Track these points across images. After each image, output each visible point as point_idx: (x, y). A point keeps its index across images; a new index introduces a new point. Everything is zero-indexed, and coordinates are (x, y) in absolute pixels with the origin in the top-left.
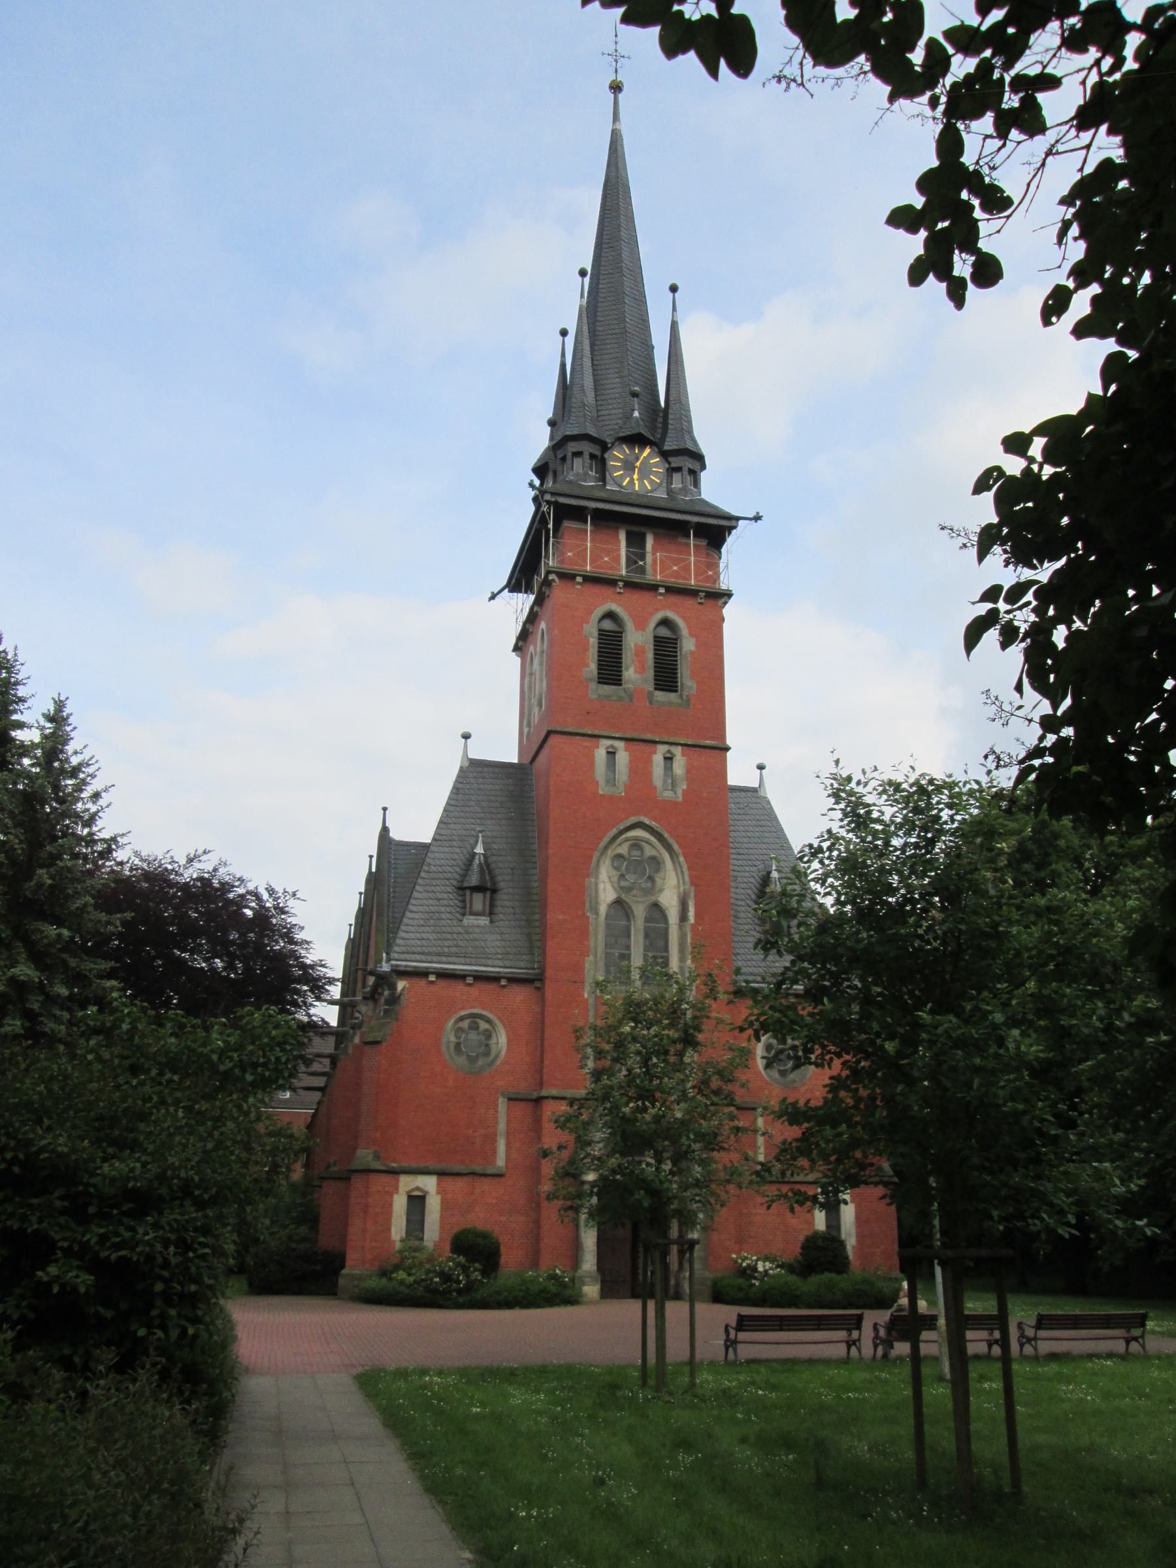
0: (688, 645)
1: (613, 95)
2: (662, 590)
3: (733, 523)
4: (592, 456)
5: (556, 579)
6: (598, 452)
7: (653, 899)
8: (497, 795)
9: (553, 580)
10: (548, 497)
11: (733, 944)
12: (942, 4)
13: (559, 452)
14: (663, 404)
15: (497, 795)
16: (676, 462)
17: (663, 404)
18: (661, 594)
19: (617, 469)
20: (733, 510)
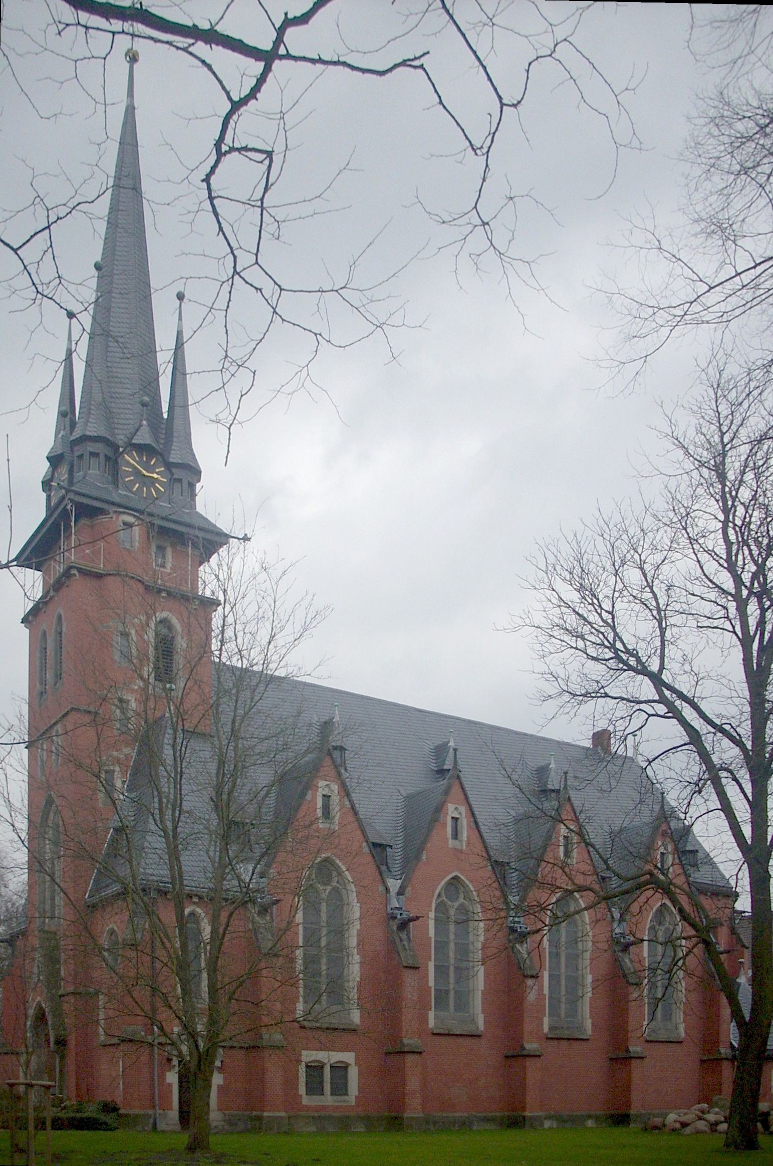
1: (128, 65)
7: (101, 272)
8: (118, 424)
9: (75, 575)
11: (116, 431)
13: (76, 448)
14: (165, 416)
15: (118, 424)
16: (178, 473)
17: (165, 416)
18: (163, 597)
19: (129, 474)
20: (223, 525)
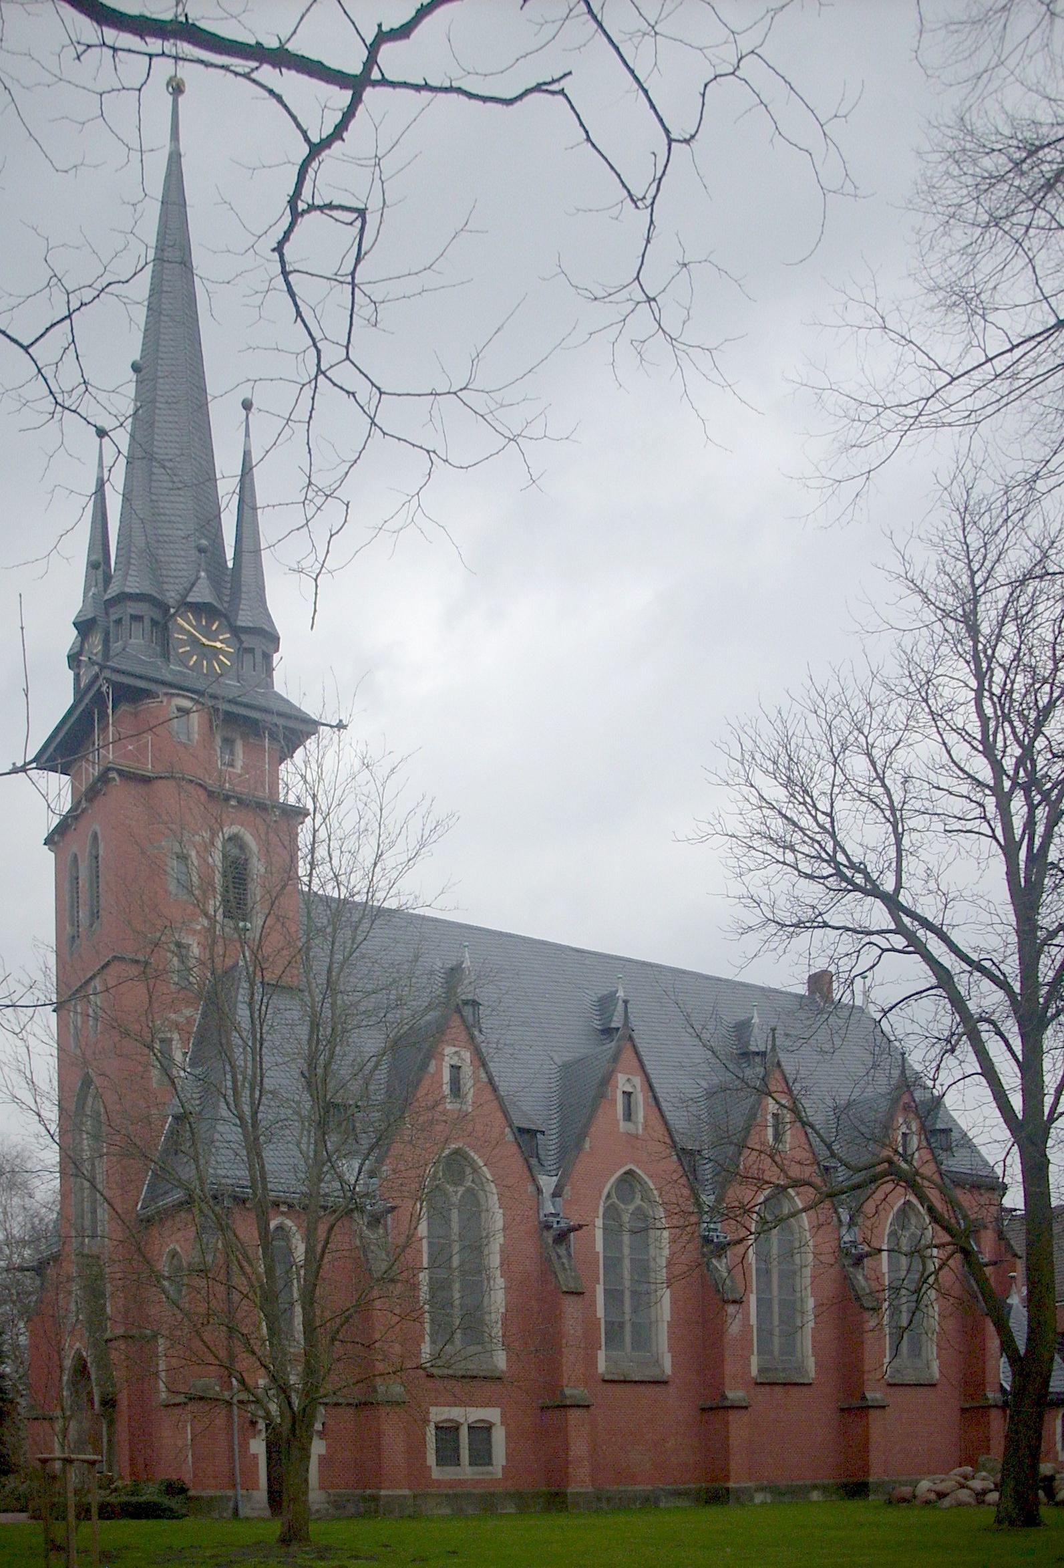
0: (257, 867)
1: (171, 98)
2: (233, 803)
3: (310, 728)
4: (154, 623)
5: (117, 779)
6: (158, 616)
10: (107, 673)
12: (570, 73)
13: (112, 611)
17: (230, 564)
18: (233, 807)
19: (183, 643)
20: (310, 708)
